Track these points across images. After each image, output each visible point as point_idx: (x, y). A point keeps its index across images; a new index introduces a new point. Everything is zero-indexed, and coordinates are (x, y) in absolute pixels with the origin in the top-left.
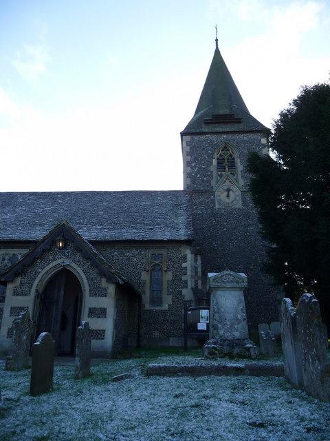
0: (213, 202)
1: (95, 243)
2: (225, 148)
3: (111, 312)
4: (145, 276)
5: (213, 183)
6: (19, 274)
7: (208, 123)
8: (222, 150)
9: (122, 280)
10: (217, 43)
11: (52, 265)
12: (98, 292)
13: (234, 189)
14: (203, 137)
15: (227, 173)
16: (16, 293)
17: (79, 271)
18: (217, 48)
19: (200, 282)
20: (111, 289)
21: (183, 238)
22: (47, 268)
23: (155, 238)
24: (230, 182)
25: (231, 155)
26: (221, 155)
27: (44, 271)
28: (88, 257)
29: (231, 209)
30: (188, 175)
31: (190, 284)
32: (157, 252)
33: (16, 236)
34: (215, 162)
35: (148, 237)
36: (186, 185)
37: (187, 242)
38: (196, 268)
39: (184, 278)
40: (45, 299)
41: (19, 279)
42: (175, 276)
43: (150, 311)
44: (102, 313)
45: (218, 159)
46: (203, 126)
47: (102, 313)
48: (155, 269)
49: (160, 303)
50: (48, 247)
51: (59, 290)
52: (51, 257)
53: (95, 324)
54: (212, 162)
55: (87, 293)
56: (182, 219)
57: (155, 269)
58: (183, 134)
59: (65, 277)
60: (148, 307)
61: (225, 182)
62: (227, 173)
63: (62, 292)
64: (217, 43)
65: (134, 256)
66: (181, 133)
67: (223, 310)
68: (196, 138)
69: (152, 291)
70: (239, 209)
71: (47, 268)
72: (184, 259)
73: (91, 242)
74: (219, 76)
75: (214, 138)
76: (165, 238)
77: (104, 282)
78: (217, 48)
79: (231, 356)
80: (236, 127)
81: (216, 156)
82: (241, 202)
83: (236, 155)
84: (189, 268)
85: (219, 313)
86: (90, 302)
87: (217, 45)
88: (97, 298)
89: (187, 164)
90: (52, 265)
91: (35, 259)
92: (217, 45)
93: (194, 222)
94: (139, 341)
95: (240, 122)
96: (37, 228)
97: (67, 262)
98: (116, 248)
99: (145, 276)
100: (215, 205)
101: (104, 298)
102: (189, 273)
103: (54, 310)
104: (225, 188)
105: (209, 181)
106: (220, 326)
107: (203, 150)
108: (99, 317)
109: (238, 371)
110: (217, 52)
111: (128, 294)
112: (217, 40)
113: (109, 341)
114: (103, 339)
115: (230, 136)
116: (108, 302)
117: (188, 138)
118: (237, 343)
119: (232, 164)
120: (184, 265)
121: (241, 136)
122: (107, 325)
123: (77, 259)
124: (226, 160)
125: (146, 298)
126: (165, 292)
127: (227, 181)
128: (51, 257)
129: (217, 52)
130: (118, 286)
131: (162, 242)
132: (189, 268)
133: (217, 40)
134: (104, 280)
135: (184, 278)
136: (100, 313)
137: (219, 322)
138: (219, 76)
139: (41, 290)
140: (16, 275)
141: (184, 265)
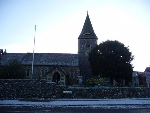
1: (61, 66)
2: (88, 42)
3: (65, 79)
4: (70, 72)
5: (85, 50)
7: (84, 36)
15: (88, 48)
16: (49, 76)
19: (80, 74)
20: (65, 76)
21: (77, 65)
23: (72, 65)
27: (54, 72)
30: (79, 49)
31: (78, 74)
32: (72, 68)
33: (45, 64)
34: (85, 45)
35: (71, 65)
36: (79, 52)
37: (78, 66)
38: (79, 71)
39: (77, 73)
41: (49, 74)
44: (63, 79)
46: (83, 36)
47: (63, 79)
48: (72, 71)
49: (29, 76)
53: (62, 81)
56: (77, 61)
57: (72, 71)
60: (70, 78)
62: (88, 48)
68: (81, 39)
69: (71, 75)
72: (77, 69)
73: (60, 66)
74: (88, 24)
75: (85, 40)
76: (74, 65)
79: (80, 85)
83: (90, 44)
84: (78, 71)
86: (61, 78)
89: (79, 46)
93: (80, 62)
96: (49, 62)
97: (57, 71)
99: (70, 72)
102: (78, 72)
109: (80, 86)
110: (88, 15)
111: (67, 76)
115: (89, 39)
116: (64, 78)
117: (79, 39)
118: (80, 84)
119: (89, 46)
120: (77, 70)
121: (91, 39)
122: (64, 81)
125: (70, 76)
126: (73, 75)
129: (88, 15)
130: (66, 75)
132: (78, 71)
134: (64, 74)
135: (77, 73)
136: (63, 79)
138: (88, 24)
141: (77, 70)
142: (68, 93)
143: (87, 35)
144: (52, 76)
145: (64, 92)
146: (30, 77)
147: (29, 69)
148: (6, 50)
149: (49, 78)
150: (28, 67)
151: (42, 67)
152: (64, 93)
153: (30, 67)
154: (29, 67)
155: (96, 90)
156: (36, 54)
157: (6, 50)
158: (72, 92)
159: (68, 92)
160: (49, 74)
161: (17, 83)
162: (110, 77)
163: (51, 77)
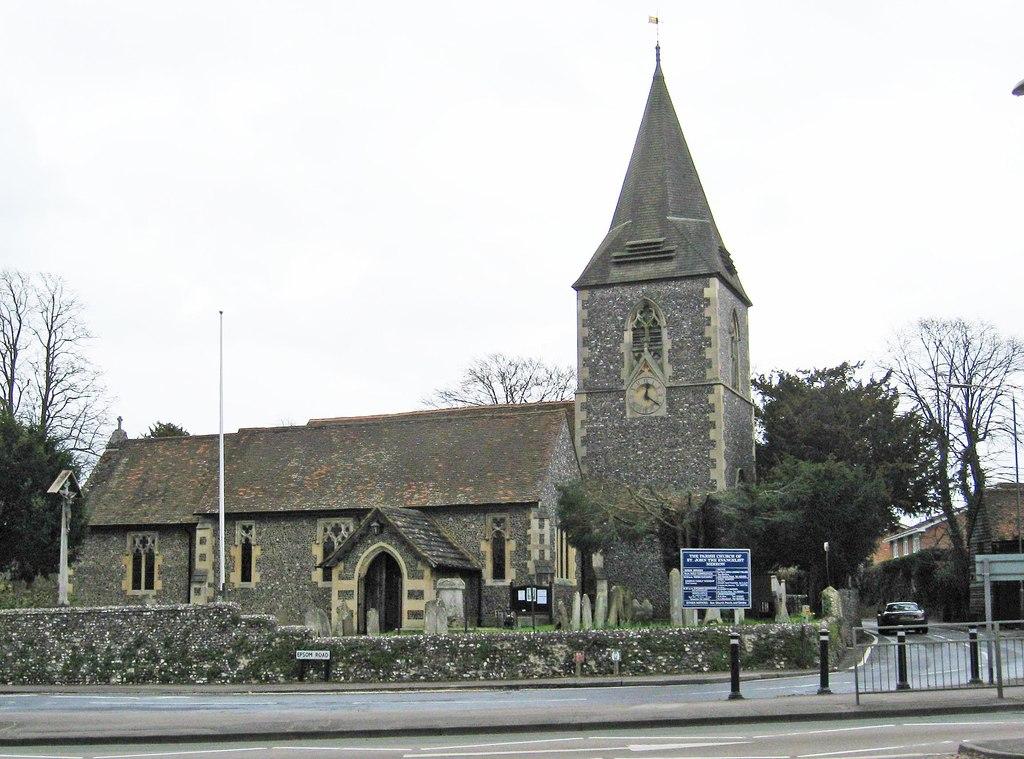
0: (622, 407)
2: (647, 307)
5: (625, 372)
7: (620, 263)
8: (641, 313)
10: (658, 55)
11: (371, 548)
12: (415, 575)
13: (656, 384)
14: (609, 292)
16: (341, 578)
17: (396, 554)
18: (658, 66)
20: (427, 572)
24: (650, 371)
25: (655, 321)
26: (638, 322)
27: (364, 557)
29: (650, 418)
32: (499, 516)
34: (628, 336)
40: (368, 582)
42: (519, 545)
43: (491, 587)
45: (634, 329)
51: (381, 573)
54: (622, 337)
58: (578, 287)
59: (385, 561)
61: (642, 371)
63: (384, 576)
64: (658, 55)
70: (662, 418)
71: (365, 554)
77: (420, 567)
78: (658, 66)
80: (667, 268)
81: (630, 325)
82: (665, 406)
83: (663, 322)
86: (408, 584)
87: (658, 60)
92: (658, 60)
94: (903, 676)
95: (670, 259)
96: (976, 381)
100: (625, 414)
104: (642, 382)
105: (617, 372)
107: (609, 315)
110: (658, 79)
112: (658, 48)
115: (654, 288)
117: (586, 294)
119: (656, 338)
121: (671, 287)
124: (647, 331)
125: (487, 573)
127: (646, 370)
133: (658, 48)
139: (362, 576)
140: (339, 560)
142: (313, 657)
143: (651, 253)
144: (356, 577)
145: (302, 655)
146: (257, 583)
147: (247, 540)
148: (120, 420)
149: (134, 588)
150: (244, 528)
151: (321, 522)
152: (301, 658)
153: (251, 527)
154: (247, 523)
155: (434, 645)
156: (245, 441)
157: (120, 420)
158: (328, 652)
159: (314, 655)
160: (530, 565)
161: (132, 621)
162: (499, 573)
163: (352, 585)
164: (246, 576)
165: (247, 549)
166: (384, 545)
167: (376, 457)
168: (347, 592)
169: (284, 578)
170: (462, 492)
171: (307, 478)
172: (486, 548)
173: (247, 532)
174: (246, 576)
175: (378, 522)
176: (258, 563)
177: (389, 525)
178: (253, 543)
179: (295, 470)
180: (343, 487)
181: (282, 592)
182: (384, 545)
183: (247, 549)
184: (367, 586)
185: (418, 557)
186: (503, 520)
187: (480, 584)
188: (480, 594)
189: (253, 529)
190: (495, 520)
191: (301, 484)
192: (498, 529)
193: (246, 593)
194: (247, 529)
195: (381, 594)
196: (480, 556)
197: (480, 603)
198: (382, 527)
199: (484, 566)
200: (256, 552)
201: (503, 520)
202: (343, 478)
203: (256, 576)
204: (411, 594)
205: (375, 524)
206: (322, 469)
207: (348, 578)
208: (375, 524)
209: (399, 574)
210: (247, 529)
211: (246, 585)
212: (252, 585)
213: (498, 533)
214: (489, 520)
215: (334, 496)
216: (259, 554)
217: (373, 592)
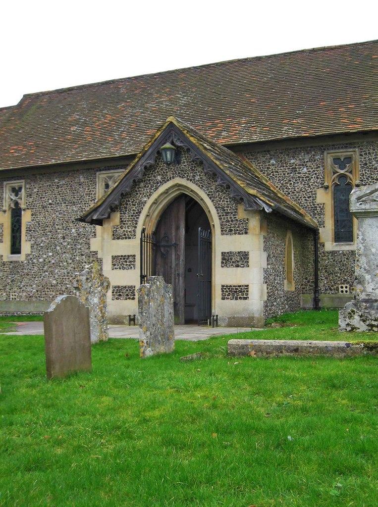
6: (116, 207)
9: (270, 206)
11: (162, 189)
12: (235, 228)
20: (254, 223)
22: (155, 196)
28: (214, 174)
32: (342, 154)
43: (333, 253)
50: (152, 162)
51: (178, 228)
52: (159, 178)
55: (217, 230)
60: (330, 245)
63: (183, 231)
65: (304, 165)
66: (25, 96)
67: (373, 250)
71: (155, 196)
85: (366, 256)
86: (222, 243)
88: (234, 236)
90: (162, 189)
91: (136, 183)
98: (272, 153)
101: (244, 236)
103: (173, 256)
106: (368, 277)
108: (237, 266)
113: (255, 303)
114: (246, 299)
123: (197, 178)
125: (327, 233)
128: (159, 178)
131: (347, 135)
137: (368, 272)
139: (150, 229)
140: (113, 209)
146: (28, 255)
147: (17, 204)
151: (101, 176)
153: (20, 188)
154: (16, 184)
163: (131, 247)
164: (16, 249)
165: (16, 214)
166: (183, 182)
167: (170, 100)
168: (125, 258)
169: (58, 248)
170: (286, 125)
171: (88, 128)
172: (324, 198)
173: (16, 195)
174: (16, 249)
175: (172, 143)
176: (29, 230)
177: (190, 148)
178: (23, 206)
179: (76, 123)
180: (129, 133)
181: (57, 265)
182: (183, 182)
183: (16, 214)
184: (156, 247)
185: (240, 198)
186: (349, 159)
187: (316, 250)
188: (316, 262)
189: (23, 190)
190: (336, 160)
191: (80, 135)
192: (342, 172)
193: (15, 265)
194: (16, 191)
195: (178, 259)
196: (317, 210)
197: (316, 275)
198: (178, 152)
199: (322, 224)
200: (26, 218)
201: (349, 159)
202: (129, 124)
203: (26, 247)
204: (228, 259)
205: (168, 145)
206: (106, 118)
207: (127, 237)
208: (168, 145)
209: (207, 226)
210: (16, 191)
211: (15, 257)
212: (21, 257)
213: (162, 356)
214: (329, 160)
215: (116, 143)
216: (30, 220)
217: (165, 257)
